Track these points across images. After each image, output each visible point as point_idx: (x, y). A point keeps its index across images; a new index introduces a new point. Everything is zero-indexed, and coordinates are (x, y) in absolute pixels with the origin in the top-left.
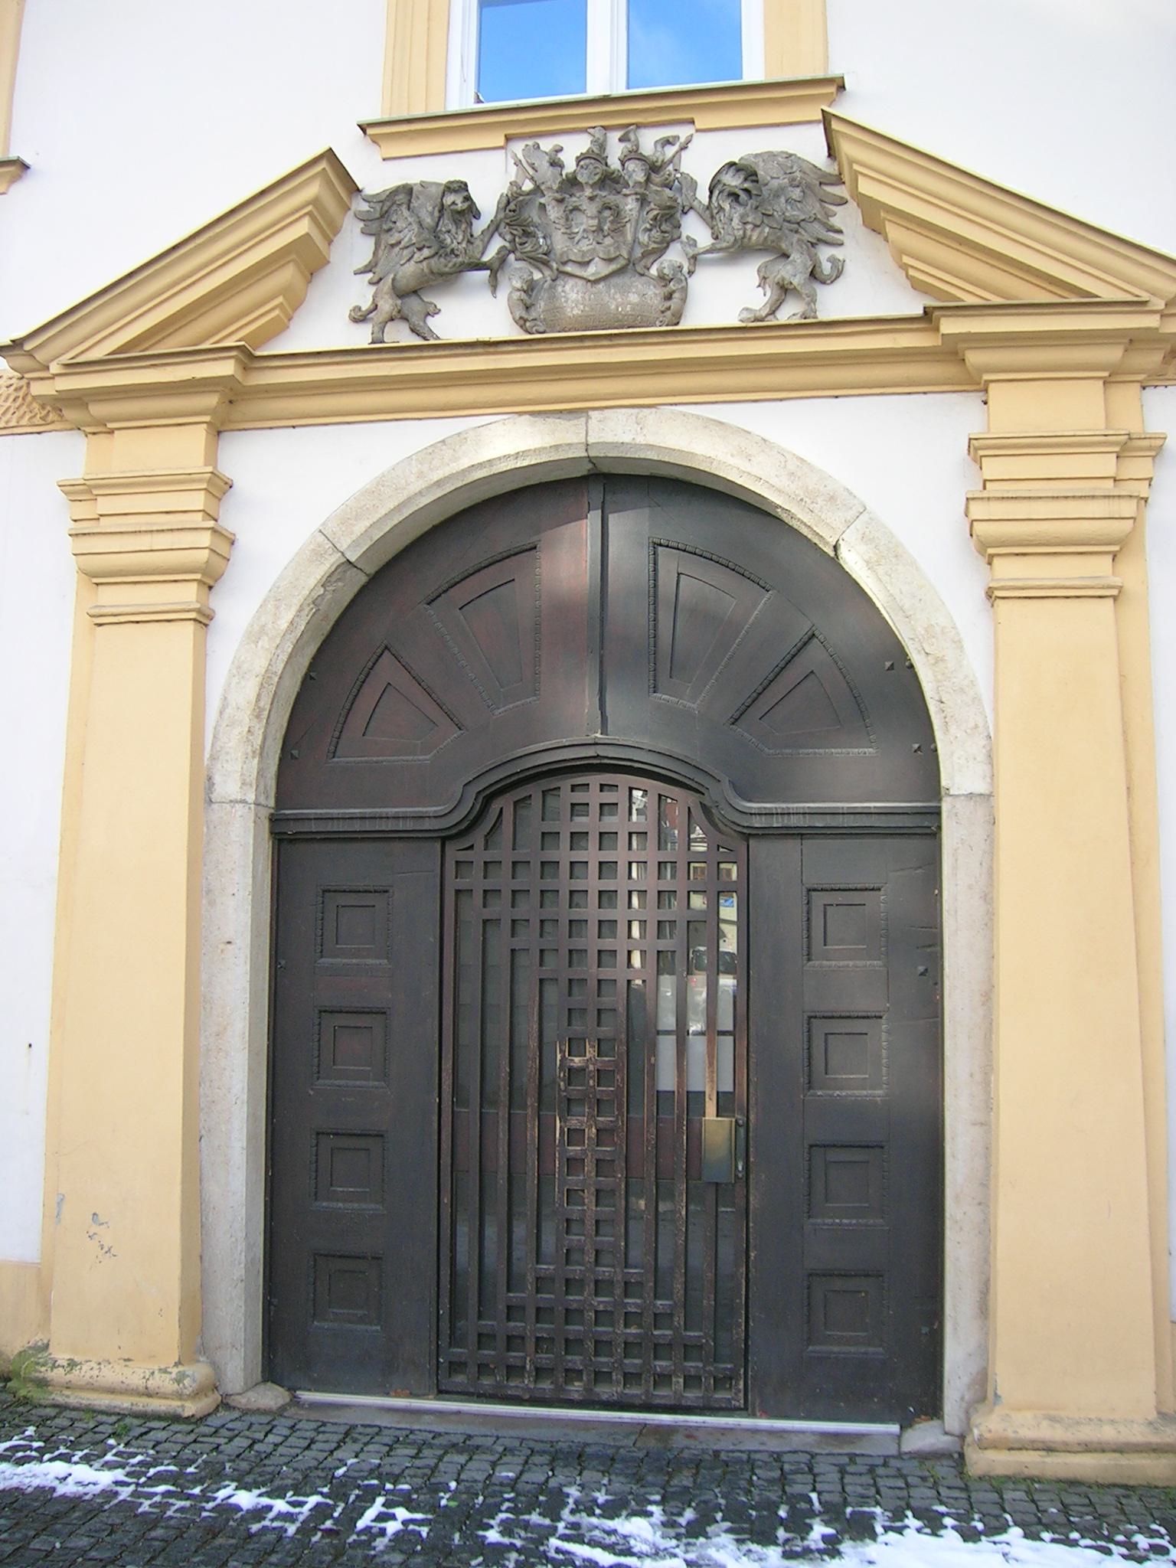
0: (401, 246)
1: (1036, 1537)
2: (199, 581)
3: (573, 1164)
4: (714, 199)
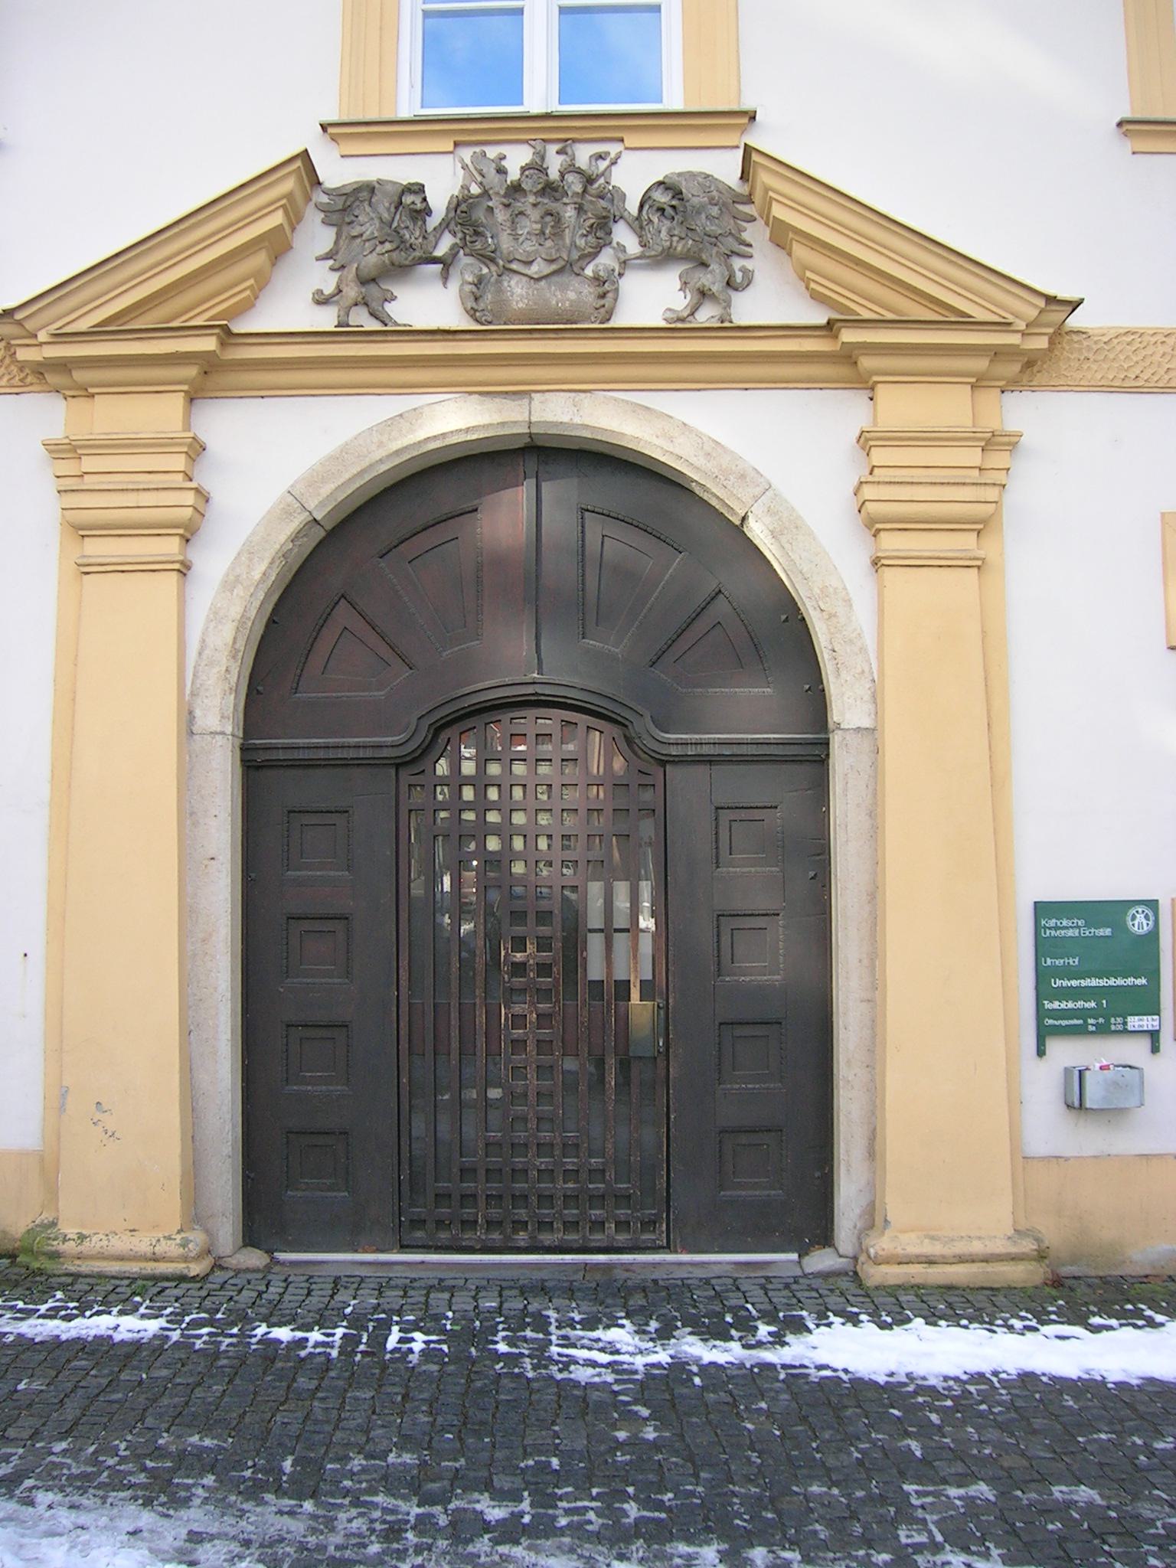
0: (364, 238)
1: (935, 1324)
2: (181, 536)
3: (518, 1045)
4: (644, 212)
